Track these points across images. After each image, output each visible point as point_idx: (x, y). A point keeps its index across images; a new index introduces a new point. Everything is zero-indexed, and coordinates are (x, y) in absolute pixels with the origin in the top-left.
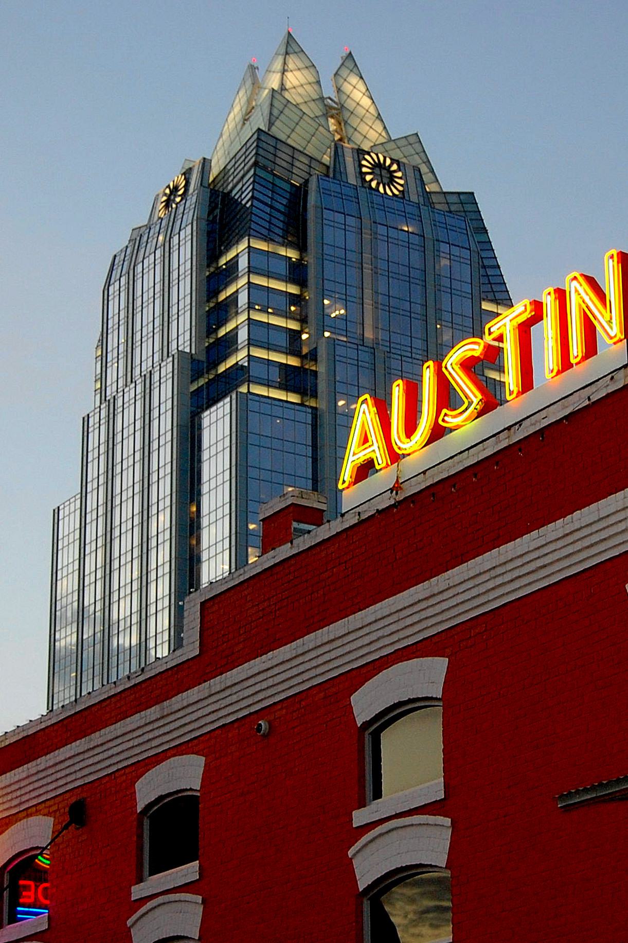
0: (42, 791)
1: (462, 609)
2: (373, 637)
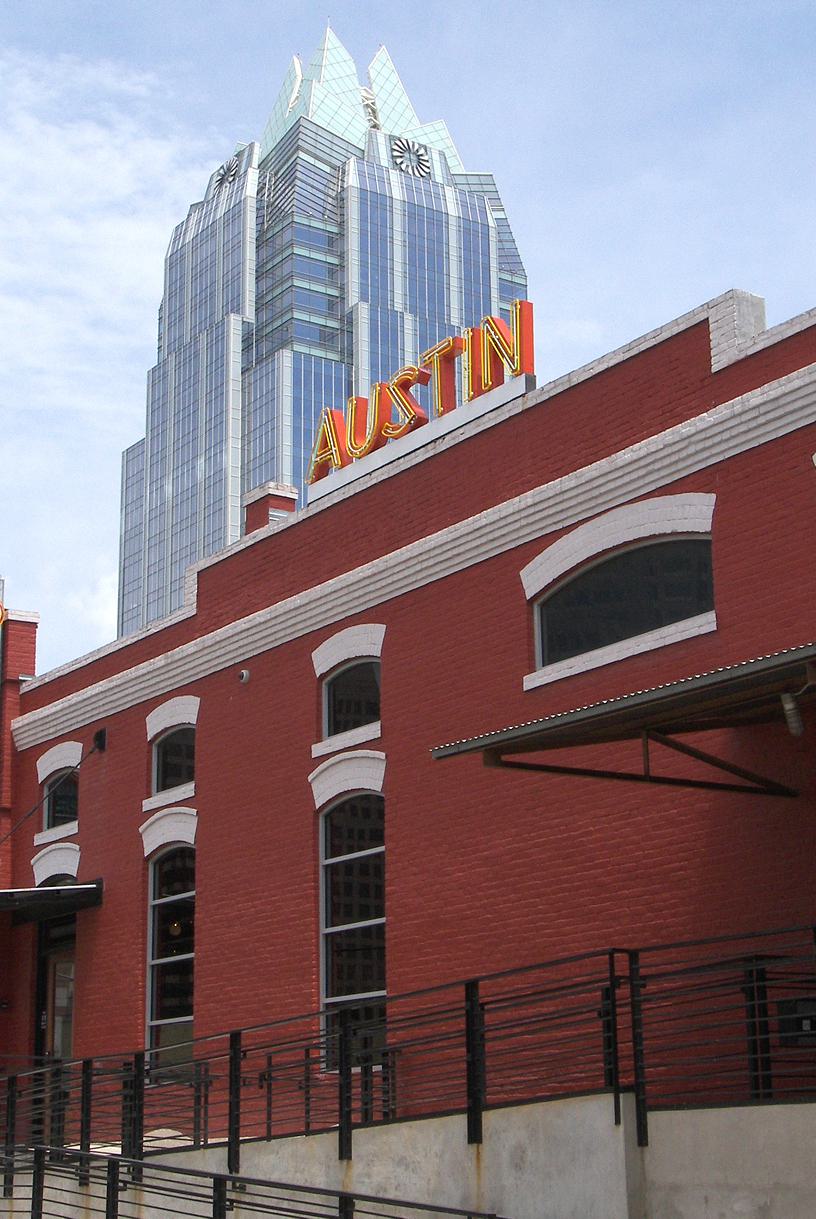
0: (74, 721)
1: (186, 675)
2: (329, 606)
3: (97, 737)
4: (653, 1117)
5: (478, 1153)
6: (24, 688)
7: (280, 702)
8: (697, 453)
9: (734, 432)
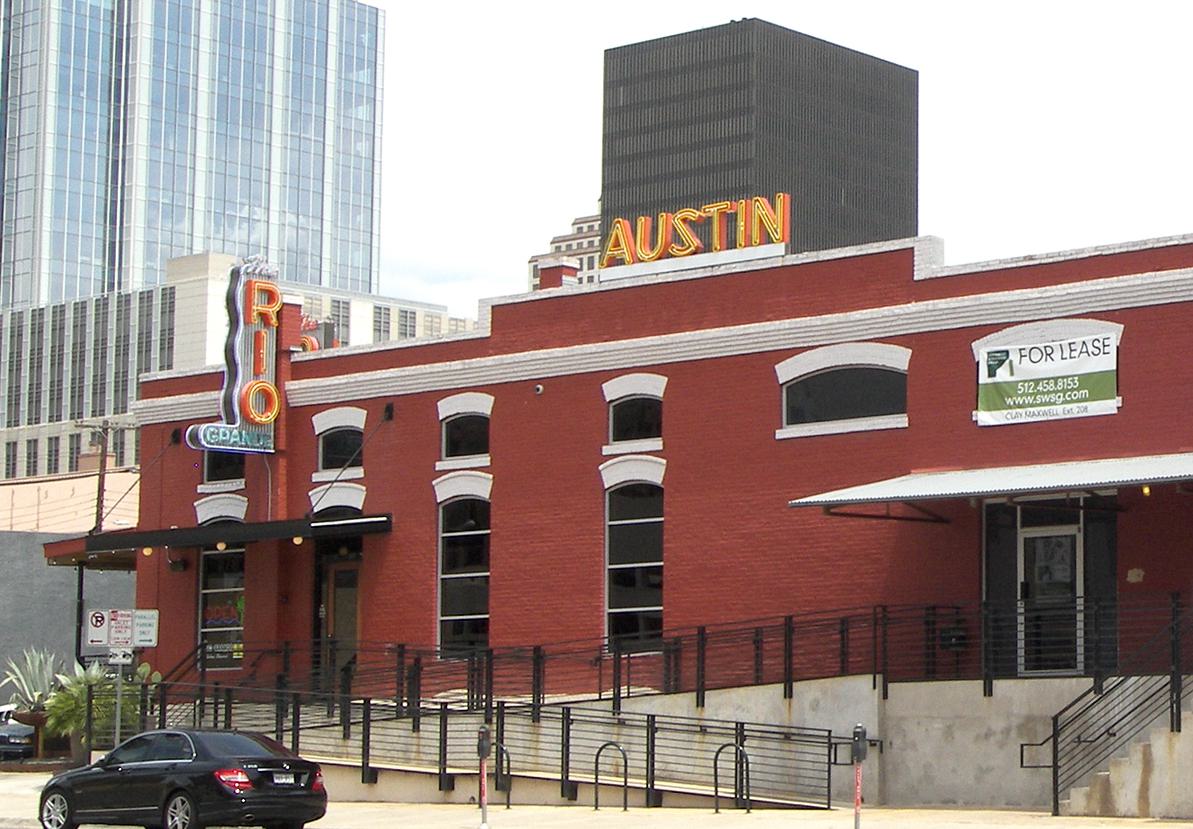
3: (385, 409)
4: (891, 686)
5: (790, 704)
6: (295, 358)
7: (570, 415)
8: (903, 324)
9: (927, 319)
